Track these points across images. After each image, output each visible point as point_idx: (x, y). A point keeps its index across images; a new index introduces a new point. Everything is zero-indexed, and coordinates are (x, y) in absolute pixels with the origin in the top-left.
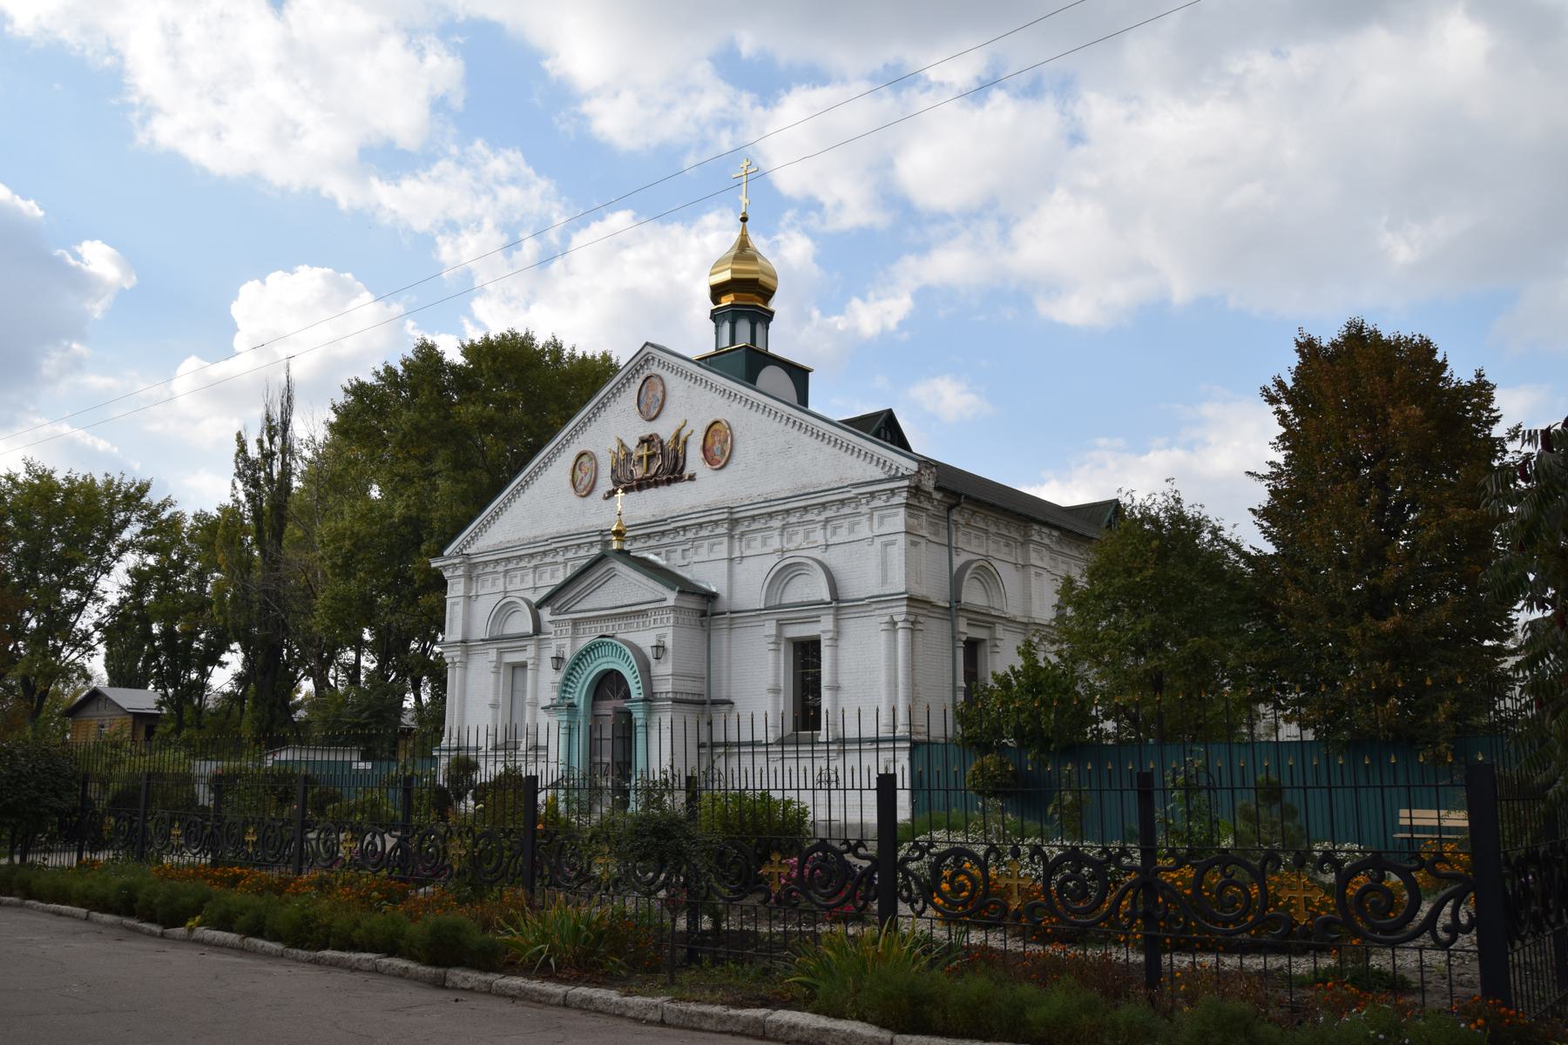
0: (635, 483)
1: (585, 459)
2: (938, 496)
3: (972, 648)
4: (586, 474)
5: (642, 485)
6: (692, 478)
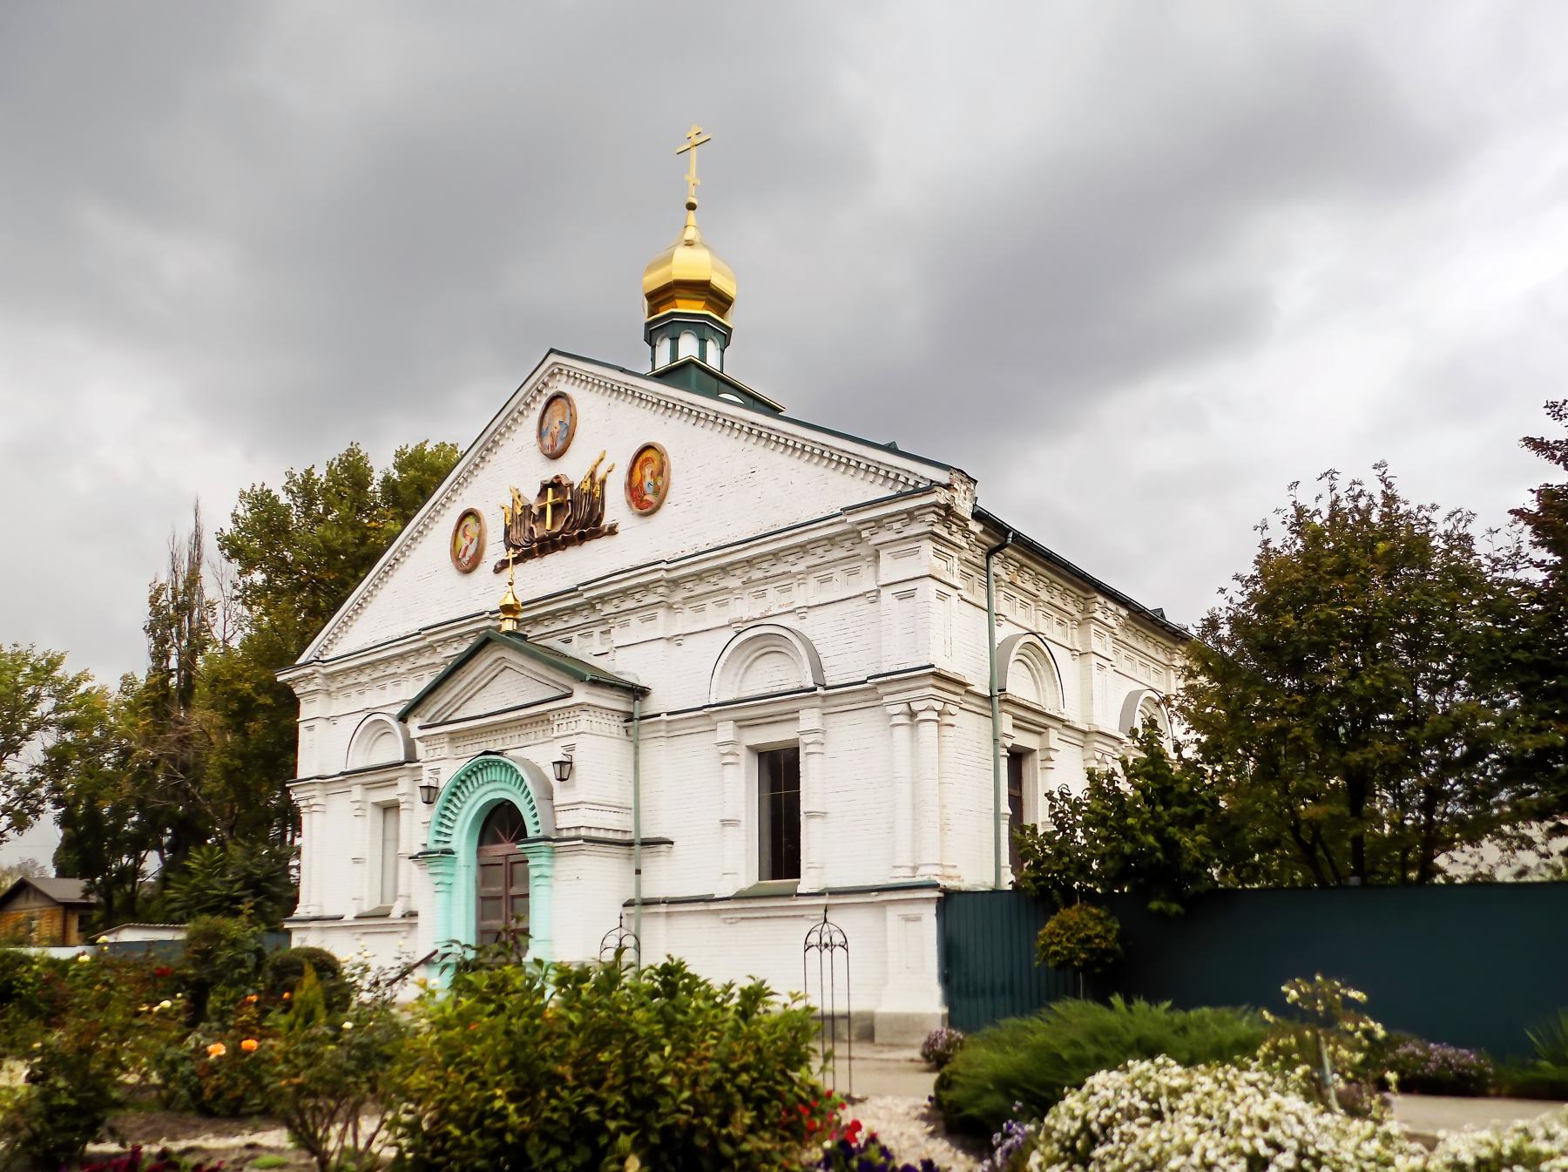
0: (535, 545)
1: (470, 521)
2: (975, 527)
3: (1017, 758)
4: (472, 540)
5: (549, 545)
6: (612, 531)
